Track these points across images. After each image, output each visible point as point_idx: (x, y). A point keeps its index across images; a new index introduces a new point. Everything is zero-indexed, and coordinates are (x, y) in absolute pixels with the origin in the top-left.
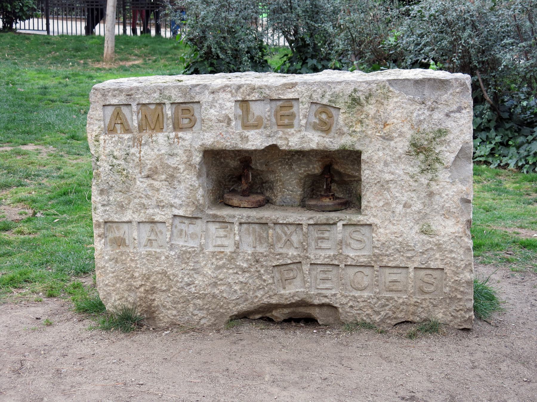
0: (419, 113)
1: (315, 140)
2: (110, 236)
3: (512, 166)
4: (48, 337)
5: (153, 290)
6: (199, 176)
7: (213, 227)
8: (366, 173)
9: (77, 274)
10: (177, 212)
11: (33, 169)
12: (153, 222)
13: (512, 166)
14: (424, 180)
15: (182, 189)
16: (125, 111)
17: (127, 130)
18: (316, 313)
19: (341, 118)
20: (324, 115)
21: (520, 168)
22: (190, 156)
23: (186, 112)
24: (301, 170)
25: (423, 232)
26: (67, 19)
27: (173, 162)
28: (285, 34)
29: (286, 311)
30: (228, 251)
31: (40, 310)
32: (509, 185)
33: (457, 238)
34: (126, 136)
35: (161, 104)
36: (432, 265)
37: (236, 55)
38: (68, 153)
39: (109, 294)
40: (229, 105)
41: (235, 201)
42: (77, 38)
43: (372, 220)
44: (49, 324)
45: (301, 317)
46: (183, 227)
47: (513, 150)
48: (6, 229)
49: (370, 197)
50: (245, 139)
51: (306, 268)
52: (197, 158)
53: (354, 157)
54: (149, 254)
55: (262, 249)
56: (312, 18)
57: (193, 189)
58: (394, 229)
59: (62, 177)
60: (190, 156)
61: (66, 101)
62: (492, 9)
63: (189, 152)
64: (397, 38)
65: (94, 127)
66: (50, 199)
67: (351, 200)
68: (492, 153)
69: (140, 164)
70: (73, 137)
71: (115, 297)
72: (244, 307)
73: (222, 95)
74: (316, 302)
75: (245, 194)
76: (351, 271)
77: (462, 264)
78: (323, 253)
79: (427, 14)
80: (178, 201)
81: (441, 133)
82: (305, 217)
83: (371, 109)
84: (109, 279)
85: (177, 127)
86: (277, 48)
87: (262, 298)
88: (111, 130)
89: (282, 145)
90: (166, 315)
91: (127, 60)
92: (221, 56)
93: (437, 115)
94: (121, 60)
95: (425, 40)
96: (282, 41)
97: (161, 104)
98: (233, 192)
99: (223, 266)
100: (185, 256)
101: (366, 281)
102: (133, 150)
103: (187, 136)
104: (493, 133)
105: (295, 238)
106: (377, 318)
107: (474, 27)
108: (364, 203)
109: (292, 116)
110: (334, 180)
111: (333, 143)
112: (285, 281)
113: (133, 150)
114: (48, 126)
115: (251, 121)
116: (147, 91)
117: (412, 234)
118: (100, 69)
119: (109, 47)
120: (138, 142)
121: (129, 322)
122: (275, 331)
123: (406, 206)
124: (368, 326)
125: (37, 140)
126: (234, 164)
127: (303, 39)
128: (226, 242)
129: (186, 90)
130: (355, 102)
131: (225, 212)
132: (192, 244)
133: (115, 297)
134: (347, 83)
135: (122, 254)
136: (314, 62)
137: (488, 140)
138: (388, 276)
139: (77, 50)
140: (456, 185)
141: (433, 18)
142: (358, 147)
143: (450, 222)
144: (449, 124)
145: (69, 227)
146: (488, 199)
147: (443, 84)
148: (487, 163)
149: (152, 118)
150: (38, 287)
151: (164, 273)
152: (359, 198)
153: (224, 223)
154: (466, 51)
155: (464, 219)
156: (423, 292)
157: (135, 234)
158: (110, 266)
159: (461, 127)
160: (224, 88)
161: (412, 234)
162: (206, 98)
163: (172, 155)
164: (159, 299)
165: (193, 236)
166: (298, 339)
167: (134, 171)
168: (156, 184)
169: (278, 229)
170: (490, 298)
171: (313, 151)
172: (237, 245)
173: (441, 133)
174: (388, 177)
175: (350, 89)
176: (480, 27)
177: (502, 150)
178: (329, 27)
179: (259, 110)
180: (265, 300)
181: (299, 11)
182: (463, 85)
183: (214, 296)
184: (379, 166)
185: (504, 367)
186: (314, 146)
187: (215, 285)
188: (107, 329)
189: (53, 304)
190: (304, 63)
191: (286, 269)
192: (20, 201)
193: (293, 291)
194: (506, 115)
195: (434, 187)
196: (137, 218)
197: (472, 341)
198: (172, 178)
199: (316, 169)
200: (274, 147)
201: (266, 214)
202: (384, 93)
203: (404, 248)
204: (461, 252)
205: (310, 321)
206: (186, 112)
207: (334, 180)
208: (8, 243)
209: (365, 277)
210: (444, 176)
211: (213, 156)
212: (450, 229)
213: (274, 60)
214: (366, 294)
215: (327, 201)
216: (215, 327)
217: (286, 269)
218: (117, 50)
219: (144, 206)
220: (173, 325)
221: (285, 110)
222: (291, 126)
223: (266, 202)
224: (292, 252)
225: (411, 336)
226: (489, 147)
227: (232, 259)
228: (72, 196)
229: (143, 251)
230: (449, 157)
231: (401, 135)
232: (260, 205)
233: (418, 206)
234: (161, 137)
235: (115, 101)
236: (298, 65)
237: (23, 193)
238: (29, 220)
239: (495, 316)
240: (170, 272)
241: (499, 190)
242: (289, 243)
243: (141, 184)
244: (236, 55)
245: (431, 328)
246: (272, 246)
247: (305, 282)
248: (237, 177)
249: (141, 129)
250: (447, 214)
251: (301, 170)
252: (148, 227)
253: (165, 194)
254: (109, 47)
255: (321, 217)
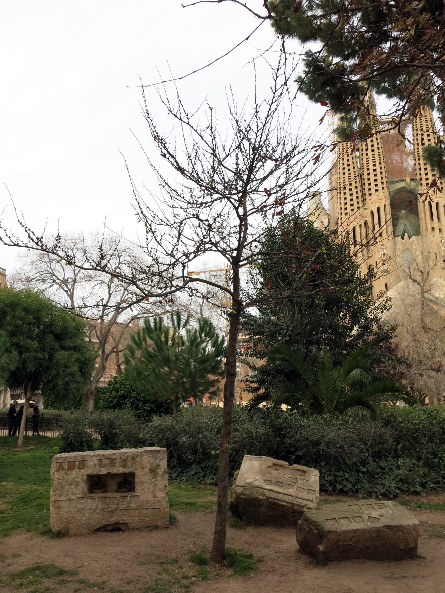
0: (152, 460)
1: (122, 470)
2: (56, 505)
3: (185, 480)
4: (32, 542)
5: (69, 523)
6: (85, 484)
7: (89, 500)
8: (137, 480)
9: (35, 524)
10: (78, 496)
11: (8, 491)
12: (70, 500)
13: (185, 480)
14: (153, 480)
15: (80, 488)
16: (63, 464)
17: (63, 470)
18: (121, 526)
19: (129, 463)
20: (124, 462)
21: (187, 480)
22: (83, 478)
23: (83, 463)
24: (117, 480)
25: (153, 497)
26: (4, 429)
27: (77, 480)
28: (100, 434)
29: (111, 527)
30: (94, 507)
31: (26, 536)
32: (183, 486)
33: (164, 498)
34: (63, 472)
35: (75, 462)
36: (157, 507)
37: (82, 443)
38: (20, 484)
39: (54, 526)
40: (96, 460)
41: (96, 491)
42: (5, 438)
43: (138, 494)
44: (31, 539)
45: (116, 528)
46: (80, 501)
47: (185, 474)
48: (3, 512)
49: (138, 487)
50: (100, 471)
51: (118, 511)
52: (85, 478)
53: (132, 475)
54: (68, 511)
55: (104, 506)
56: (111, 427)
57: (84, 488)
58: (145, 496)
59: (20, 493)
60: (83, 478)
61: (13, 465)
62: (176, 424)
63: (83, 476)
64: (143, 435)
65: (53, 470)
66: (17, 501)
67: (132, 489)
68: (178, 476)
69: (67, 481)
70: (20, 479)
71: (56, 526)
72: (98, 526)
73: (94, 458)
74: (121, 522)
75: (99, 489)
76: (132, 511)
77: (165, 506)
78: (123, 506)
79: (154, 426)
80: (78, 492)
81: (158, 466)
82: (118, 495)
83: (138, 460)
84: (54, 520)
85: (79, 468)
86: (97, 439)
87: (104, 522)
88: (58, 470)
89: (111, 472)
90: (73, 531)
91: (28, 446)
92: (76, 444)
93: (157, 461)
94: (25, 447)
95: (154, 435)
96: (99, 437)
97: (75, 462)
98: (95, 489)
99: (92, 513)
100: (80, 510)
101: (137, 514)
102: (65, 476)
103: (82, 471)
104: (178, 468)
105: (115, 502)
106: (140, 526)
107: (170, 430)
108: (136, 489)
109: (115, 463)
110: (127, 483)
111: (127, 471)
112: (111, 517)
113: (65, 476)
114: (8, 475)
115: (103, 465)
116: (70, 458)
117: (151, 498)
118: (16, 451)
119: (20, 441)
120: (66, 474)
121: (61, 535)
122: (108, 534)
123: (149, 489)
124: (137, 529)
125: (6, 481)
126: (96, 479)
127: (107, 436)
128: (93, 505)
129: (83, 457)
130: (133, 458)
131: (93, 495)
132: (82, 506)
133: (56, 526)
134: (131, 452)
135: (59, 511)
136: (111, 444)
137: (176, 471)
138: (144, 512)
139: (5, 443)
140: (163, 482)
141: (156, 428)
142: (134, 472)
143: (161, 493)
144: (161, 463)
145: (28, 510)
146: (176, 491)
147: (158, 451)
148: (176, 479)
149: (72, 466)
150: (23, 529)
151: (73, 517)
152: (134, 488)
153: (93, 498)
154: (168, 439)
155: (165, 492)
156: (154, 516)
157: (64, 504)
158: (55, 516)
159: (164, 464)
160: (94, 456)
161: (151, 498)
162: (89, 459)
163: (77, 477)
164: (70, 526)
165: (83, 504)
166: (115, 536)
167: (65, 483)
168: (72, 487)
169: (110, 499)
170: (175, 519)
171: (121, 474)
172: (97, 505)
173: (158, 466)
174: (143, 480)
175: (132, 454)
176: (172, 430)
177: (181, 474)
178: (117, 431)
179: (105, 462)
180: (105, 523)
181: (106, 425)
182: (164, 451)
183: (89, 523)
184: (140, 477)
185: (178, 536)
186: (121, 472)
187: (89, 519)
188: (53, 538)
189: (30, 534)
190: (107, 445)
191: (112, 512)
192: (6, 503)
193: (114, 519)
194: (183, 462)
195: (157, 482)
196: (65, 499)
197: (169, 531)
198: (77, 485)
199: (121, 479)
200: (109, 473)
201: (106, 495)
202: (141, 455)
203: (148, 502)
204: (165, 504)
205: (119, 530)
206: (83, 463)
207: (127, 483)
208: (6, 517)
209: (136, 513)
210: (159, 479)
211: (90, 477)
212: (161, 495)
213: (95, 445)
214: (137, 518)
215: (125, 489)
216: (88, 534)
217: (112, 512)
218: (24, 443)
219: (67, 495)
220: (75, 534)
221: (112, 461)
222: (114, 466)
223: (105, 491)
224: (114, 506)
225: (150, 531)
226: (177, 473)
227: (95, 510)
228: (26, 500)
229: (66, 510)
230: (161, 473)
231: (147, 467)
232: (104, 492)
233: (152, 489)
234: (74, 472)
235: (60, 461)
236: (105, 446)
237: (6, 500)
238: (11, 509)
239: (176, 524)
240: (75, 516)
241: (180, 488)
242: (113, 503)
243: (67, 487)
244: (82, 443)
245: (157, 528)
246: (108, 505)
247: (118, 516)
248: (96, 483)
249: (68, 469)
250: (161, 491)
251: (117, 480)
252: (68, 502)
253: (75, 490)
254: (20, 441)
255: (123, 494)
